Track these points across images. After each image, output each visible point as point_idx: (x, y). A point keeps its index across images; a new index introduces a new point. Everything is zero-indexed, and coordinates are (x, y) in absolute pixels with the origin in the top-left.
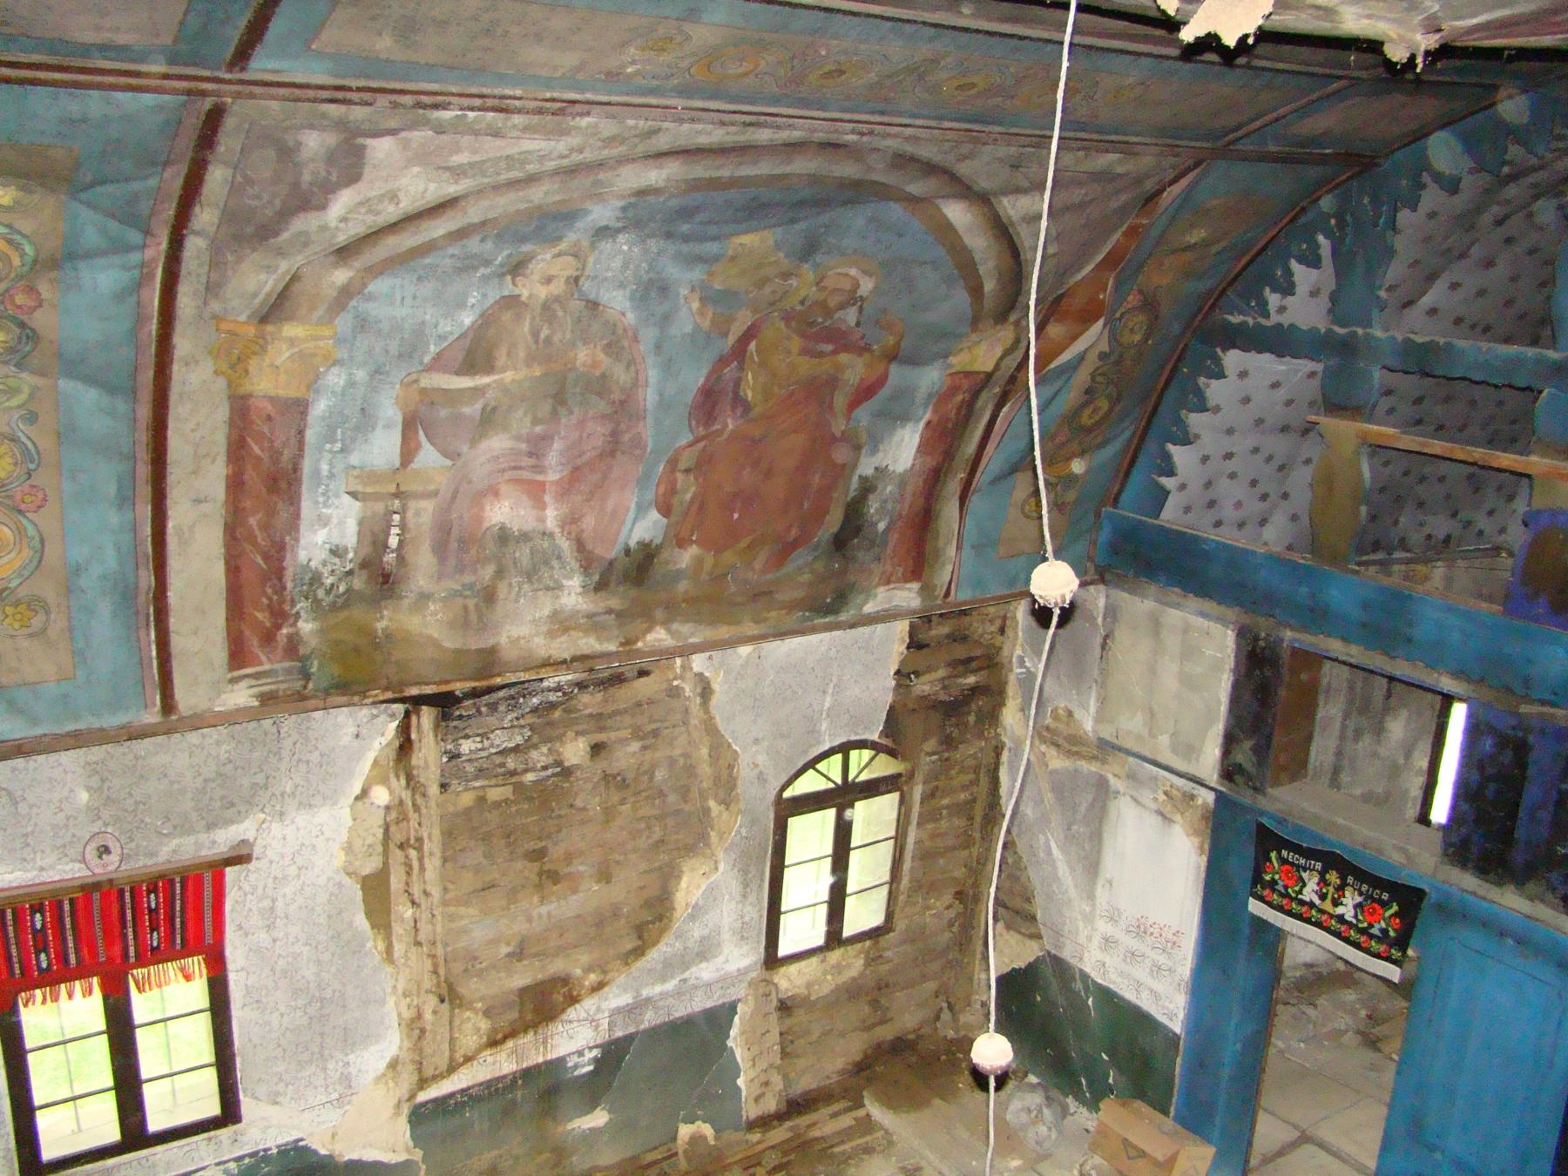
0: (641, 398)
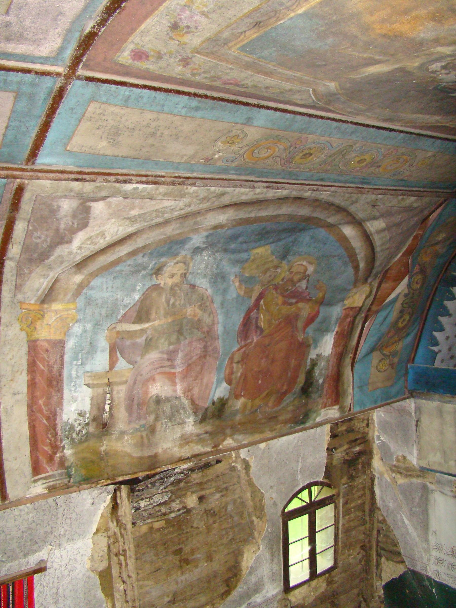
0: (216, 329)
